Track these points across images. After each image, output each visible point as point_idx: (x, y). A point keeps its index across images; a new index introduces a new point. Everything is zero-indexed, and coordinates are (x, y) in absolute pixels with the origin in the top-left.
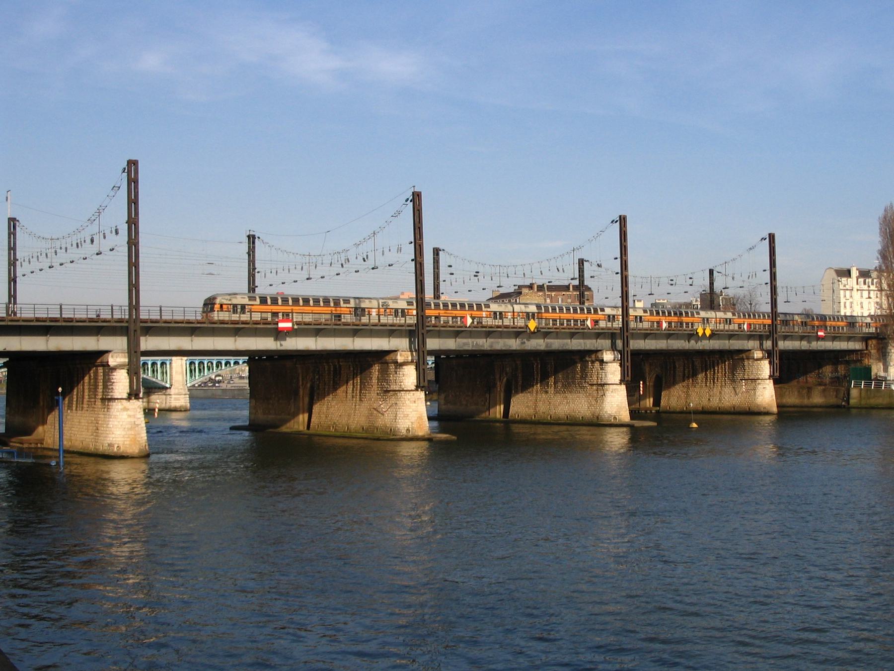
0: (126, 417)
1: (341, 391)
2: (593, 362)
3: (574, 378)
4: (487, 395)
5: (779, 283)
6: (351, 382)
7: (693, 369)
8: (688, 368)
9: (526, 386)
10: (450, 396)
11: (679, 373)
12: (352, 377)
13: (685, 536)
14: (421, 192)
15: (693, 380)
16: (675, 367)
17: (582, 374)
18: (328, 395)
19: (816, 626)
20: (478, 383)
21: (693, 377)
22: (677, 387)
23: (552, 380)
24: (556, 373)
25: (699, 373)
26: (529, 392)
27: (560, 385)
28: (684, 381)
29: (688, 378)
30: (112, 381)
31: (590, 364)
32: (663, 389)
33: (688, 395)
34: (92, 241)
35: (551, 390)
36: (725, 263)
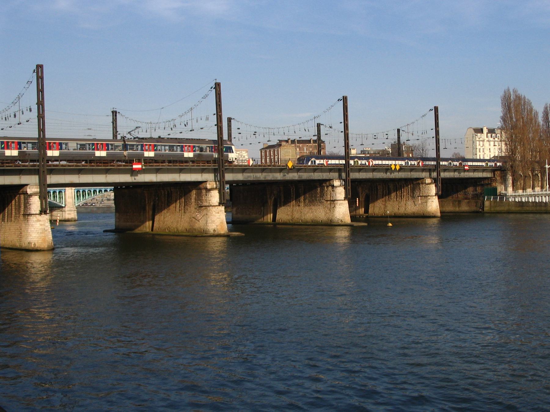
0: (39, 225)
2: (327, 187)
4: (262, 208)
6: (179, 201)
9: (286, 202)
11: (380, 192)
15: (388, 197)
17: (321, 194)
22: (379, 201)
23: (302, 199)
24: (304, 194)
27: (307, 201)
28: (383, 198)
29: (386, 196)
30: (30, 203)
31: (326, 188)
34: (15, 116)
35: (302, 204)
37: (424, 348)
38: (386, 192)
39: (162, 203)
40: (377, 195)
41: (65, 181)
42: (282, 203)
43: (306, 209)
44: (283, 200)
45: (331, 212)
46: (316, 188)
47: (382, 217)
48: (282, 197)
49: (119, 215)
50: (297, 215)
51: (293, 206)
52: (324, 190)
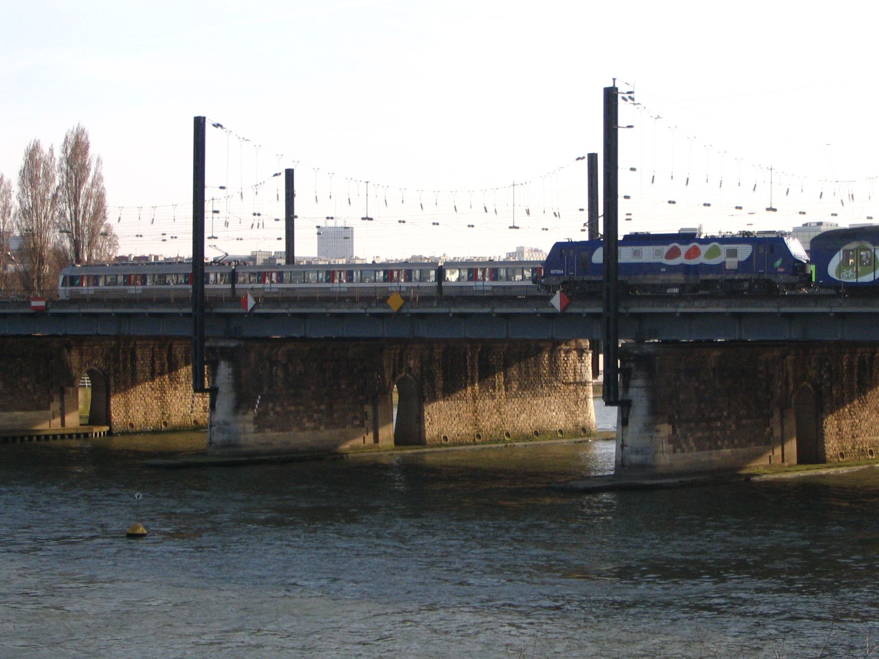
2: (567, 352)
3: (538, 375)
4: (368, 409)
8: (161, 359)
10: (272, 414)
11: (143, 364)
13: (441, 581)
16: (134, 358)
19: (693, 582)
21: (170, 371)
22: (139, 388)
23: (500, 378)
24: (506, 366)
25: (181, 367)
27: (515, 385)
28: (153, 380)
29: (161, 374)
31: (563, 355)
32: (112, 393)
33: (164, 404)
36: (213, 199)
38: (162, 365)
39: (843, 386)
40: (134, 373)
41: (189, 233)
42: (439, 394)
43: (512, 407)
45: (580, 410)
46: (539, 350)
48: (439, 374)
49: (674, 431)
50: (489, 423)
51: (475, 399)
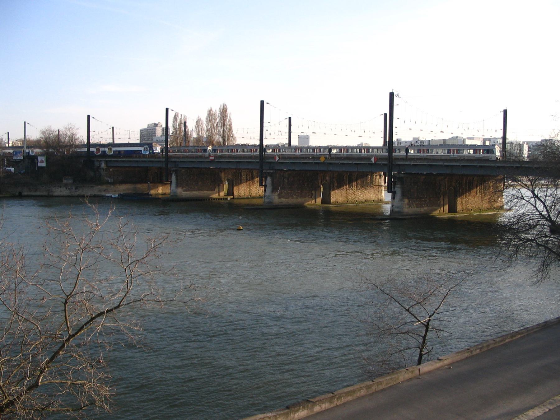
1: (473, 192)
2: (376, 176)
4: (313, 192)
5: (10, 137)
6: (479, 187)
7: (252, 177)
9: (340, 186)
11: (244, 177)
12: (479, 185)
14: (264, 101)
15: (252, 182)
16: (241, 175)
17: (371, 181)
18: (466, 193)
20: (306, 185)
23: (355, 184)
26: (342, 190)
27: (359, 186)
28: (247, 182)
29: (249, 180)
33: (250, 190)
35: (355, 188)
37: (201, 313)
38: (250, 178)
40: (241, 180)
43: (358, 193)
44: (336, 185)
47: (248, 198)
49: (409, 202)
50: (351, 197)
52: (373, 178)
